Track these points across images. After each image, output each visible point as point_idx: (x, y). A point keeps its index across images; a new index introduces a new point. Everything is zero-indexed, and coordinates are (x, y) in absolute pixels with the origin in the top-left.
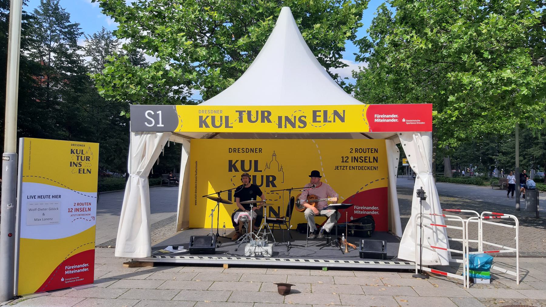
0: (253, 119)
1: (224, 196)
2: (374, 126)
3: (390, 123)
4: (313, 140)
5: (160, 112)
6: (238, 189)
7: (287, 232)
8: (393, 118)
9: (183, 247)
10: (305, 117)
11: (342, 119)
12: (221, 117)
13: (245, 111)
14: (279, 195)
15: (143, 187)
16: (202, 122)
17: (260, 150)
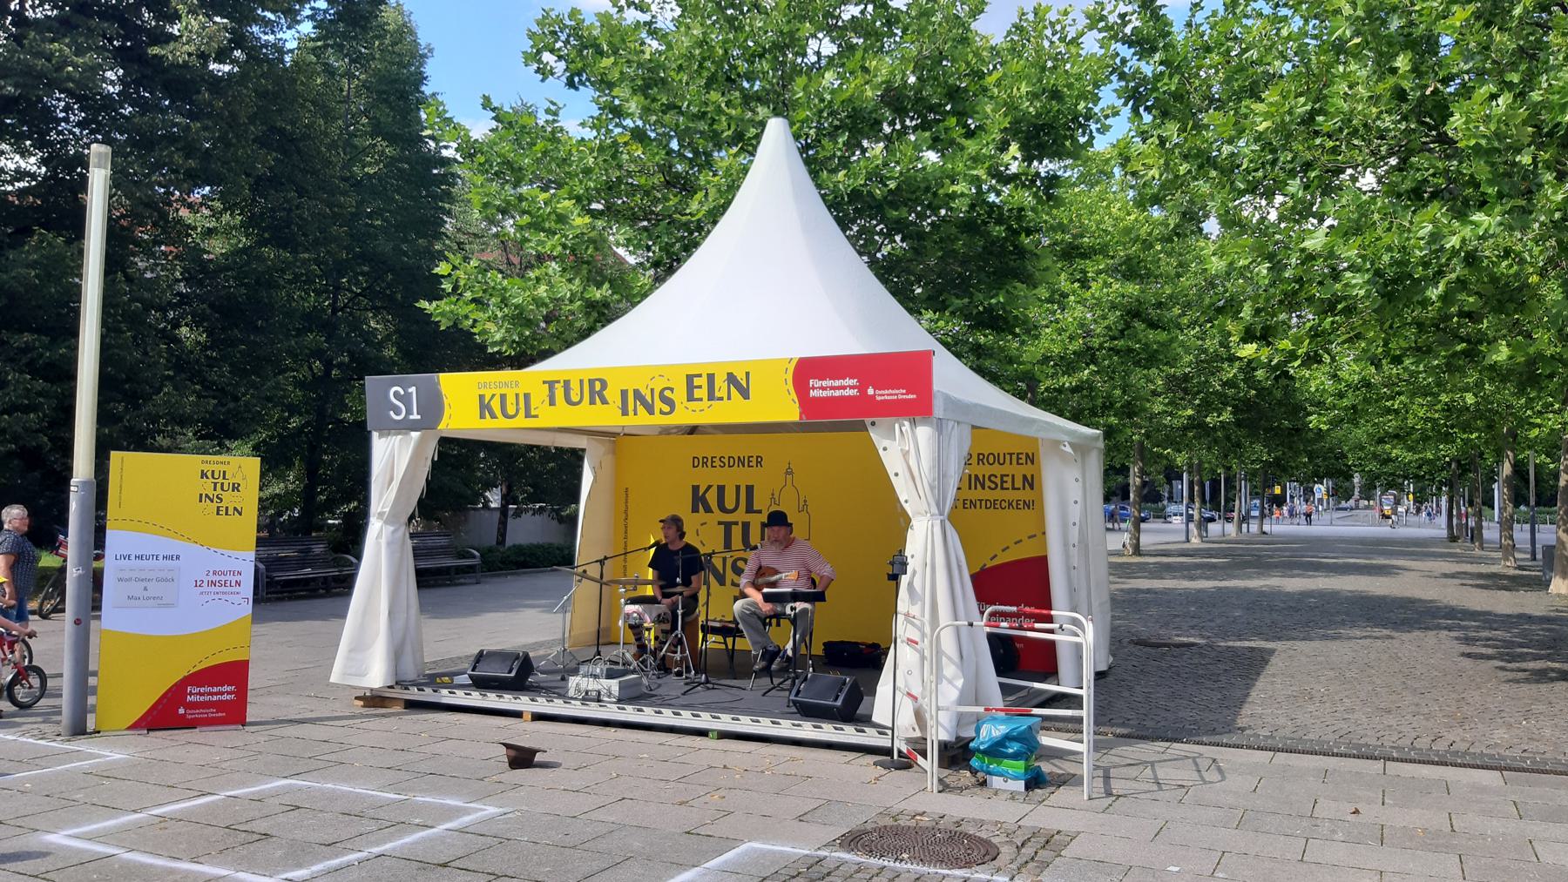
5: (413, 390)
10: (672, 390)
11: (745, 393)
15: (389, 544)
16: (485, 408)
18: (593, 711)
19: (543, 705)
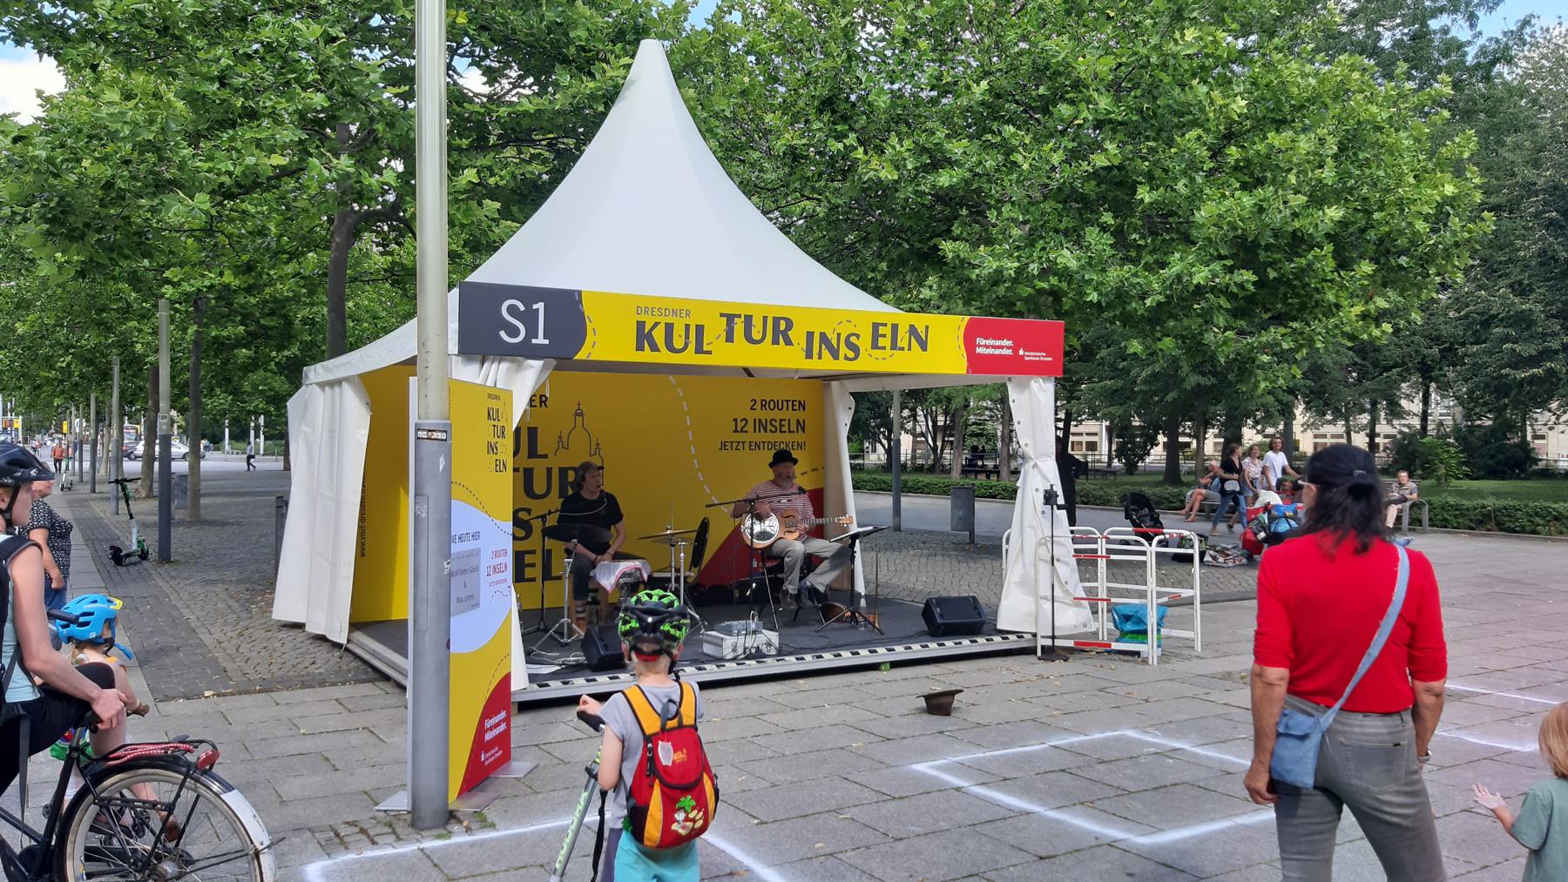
0: (756, 336)
2: (977, 363)
3: (1000, 356)
5: (540, 306)
10: (858, 336)
12: (687, 327)
18: (752, 668)
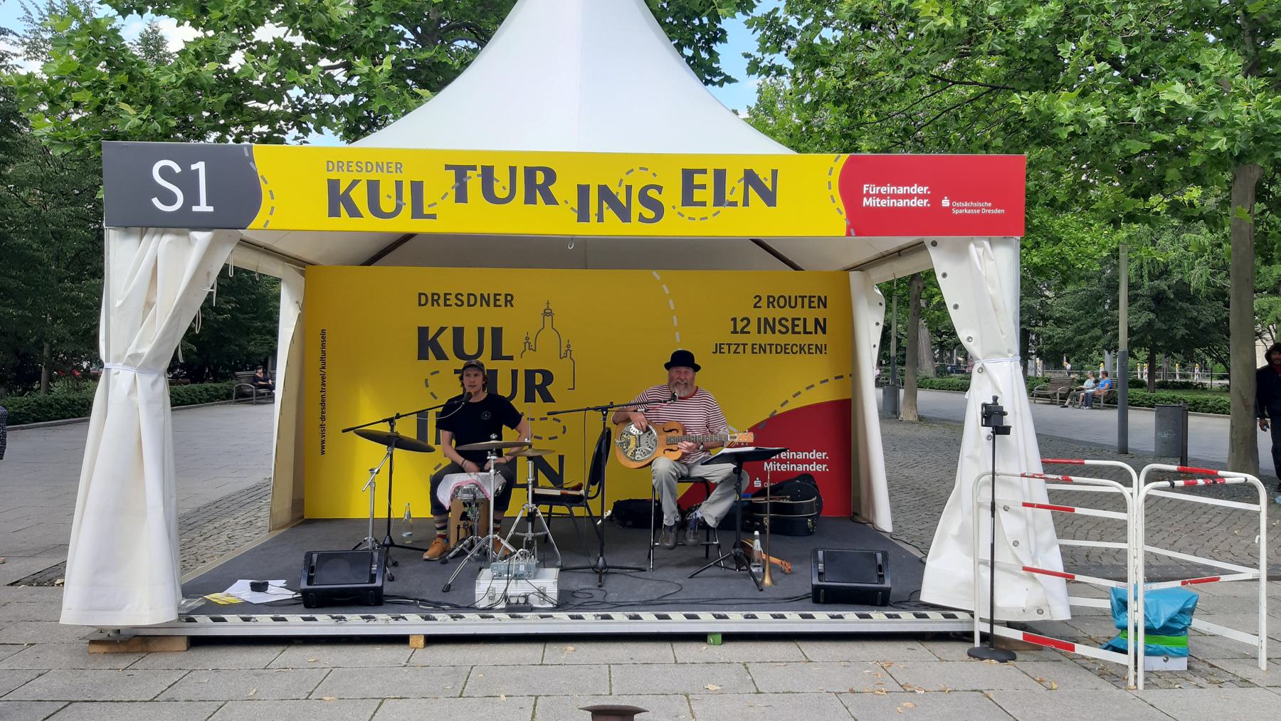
0: (500, 191)
1: (407, 429)
3: (906, 209)
4: (655, 273)
5: (200, 166)
6: (450, 406)
7: (607, 537)
8: (914, 196)
9: (282, 582)
10: (659, 189)
11: (769, 198)
12: (399, 185)
13: (474, 168)
14: (562, 424)
15: (149, 403)
16: (338, 200)
17: (509, 300)
18: (530, 624)
19: (444, 624)
